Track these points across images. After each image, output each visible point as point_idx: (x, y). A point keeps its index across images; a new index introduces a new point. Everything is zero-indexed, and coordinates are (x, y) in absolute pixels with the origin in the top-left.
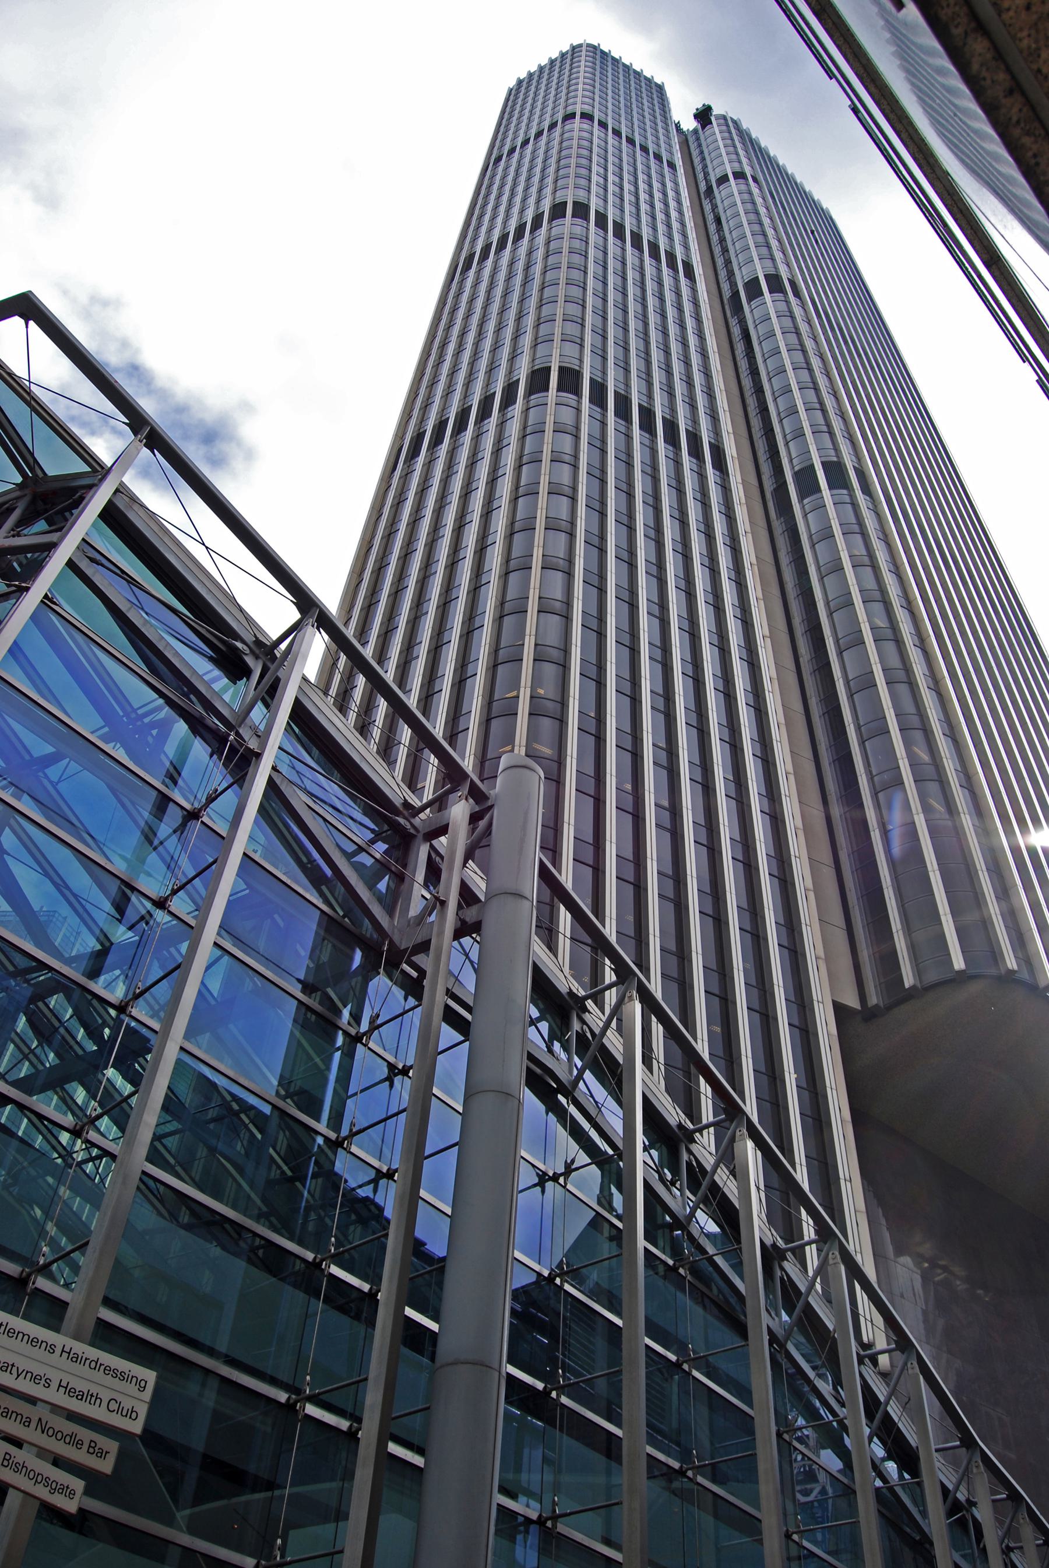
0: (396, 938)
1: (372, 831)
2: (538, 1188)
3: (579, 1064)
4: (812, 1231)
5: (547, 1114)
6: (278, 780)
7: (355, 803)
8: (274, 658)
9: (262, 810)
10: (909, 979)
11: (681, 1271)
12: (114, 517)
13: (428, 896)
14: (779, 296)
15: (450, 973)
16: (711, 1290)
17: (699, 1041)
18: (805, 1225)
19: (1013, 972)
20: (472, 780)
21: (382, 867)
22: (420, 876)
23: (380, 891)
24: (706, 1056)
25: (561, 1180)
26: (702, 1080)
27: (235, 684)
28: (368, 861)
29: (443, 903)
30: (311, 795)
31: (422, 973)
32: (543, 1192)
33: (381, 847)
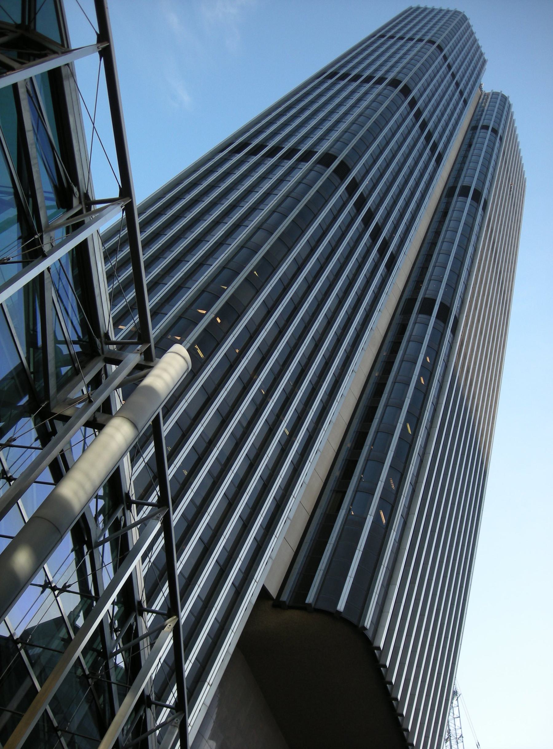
0: (52, 404)
1: (79, 337)
2: (41, 589)
3: (107, 535)
4: (173, 700)
5: (72, 551)
6: (46, 275)
7: (79, 313)
8: (89, 209)
9: (26, 287)
10: (310, 599)
11: (90, 680)
12: (56, 81)
13: (85, 392)
14: (475, 204)
15: (70, 442)
16: (99, 698)
17: (179, 562)
18: (171, 695)
19: (365, 629)
20: (150, 346)
21: (71, 360)
22: (88, 379)
23: (60, 371)
24: (178, 572)
25: (56, 592)
26: (167, 584)
27: (59, 209)
28: (65, 351)
29: (90, 402)
30: (59, 296)
31: (54, 432)
32: (42, 592)
33: (77, 348)
